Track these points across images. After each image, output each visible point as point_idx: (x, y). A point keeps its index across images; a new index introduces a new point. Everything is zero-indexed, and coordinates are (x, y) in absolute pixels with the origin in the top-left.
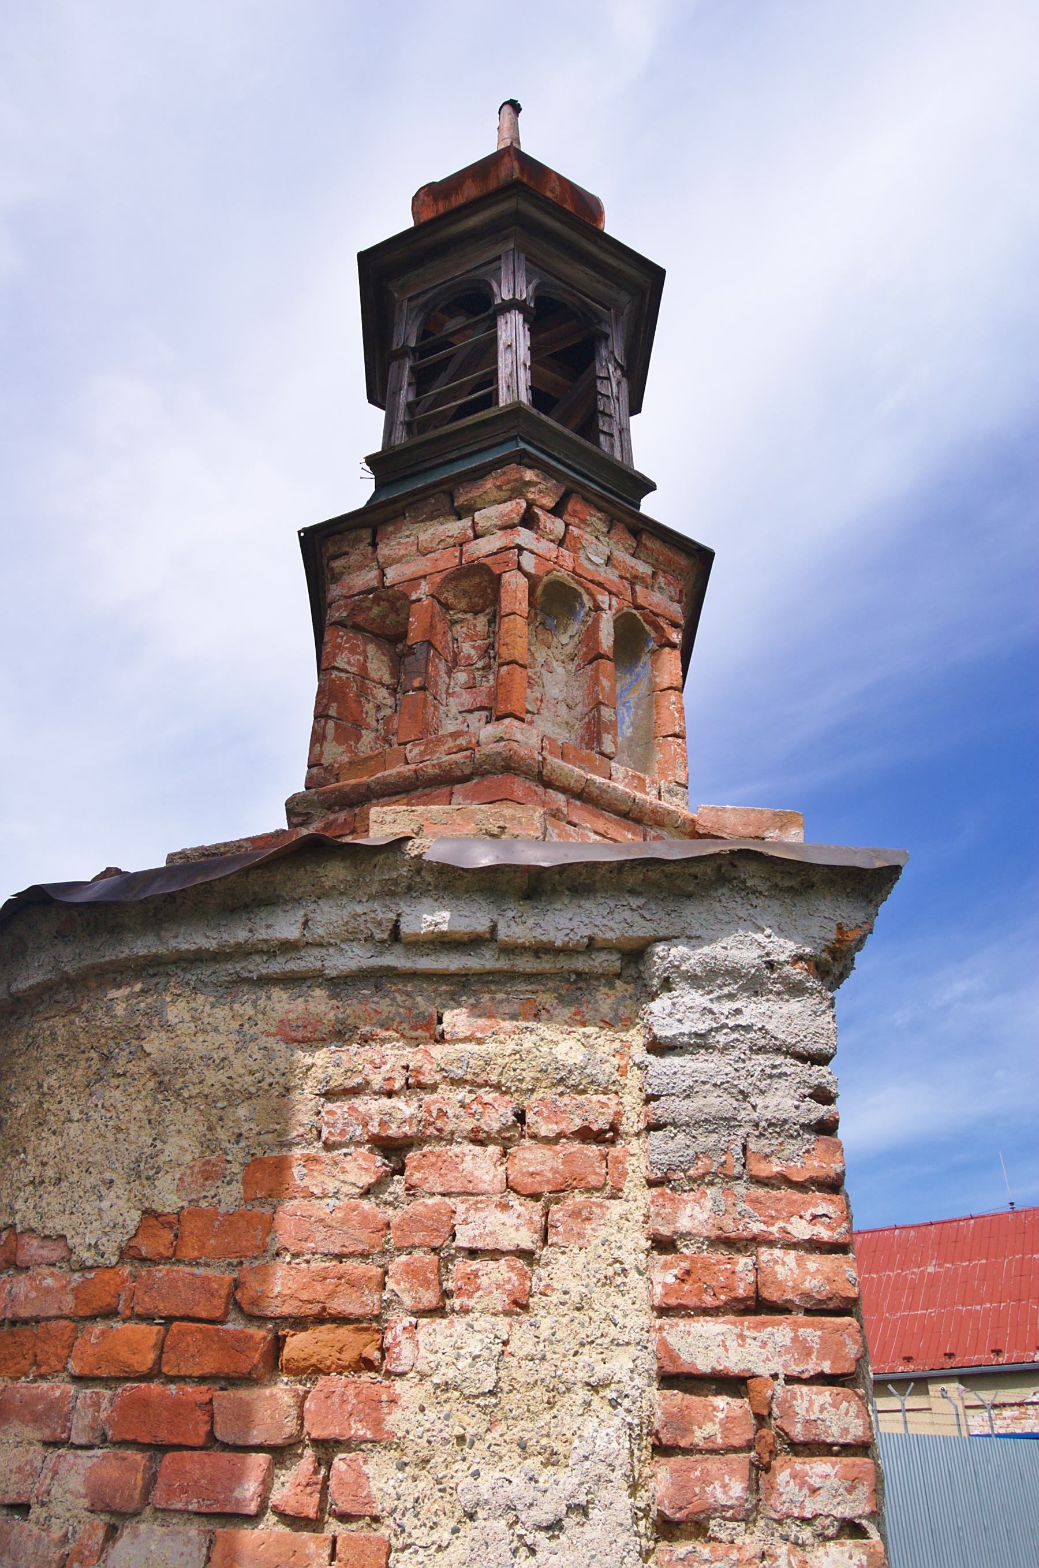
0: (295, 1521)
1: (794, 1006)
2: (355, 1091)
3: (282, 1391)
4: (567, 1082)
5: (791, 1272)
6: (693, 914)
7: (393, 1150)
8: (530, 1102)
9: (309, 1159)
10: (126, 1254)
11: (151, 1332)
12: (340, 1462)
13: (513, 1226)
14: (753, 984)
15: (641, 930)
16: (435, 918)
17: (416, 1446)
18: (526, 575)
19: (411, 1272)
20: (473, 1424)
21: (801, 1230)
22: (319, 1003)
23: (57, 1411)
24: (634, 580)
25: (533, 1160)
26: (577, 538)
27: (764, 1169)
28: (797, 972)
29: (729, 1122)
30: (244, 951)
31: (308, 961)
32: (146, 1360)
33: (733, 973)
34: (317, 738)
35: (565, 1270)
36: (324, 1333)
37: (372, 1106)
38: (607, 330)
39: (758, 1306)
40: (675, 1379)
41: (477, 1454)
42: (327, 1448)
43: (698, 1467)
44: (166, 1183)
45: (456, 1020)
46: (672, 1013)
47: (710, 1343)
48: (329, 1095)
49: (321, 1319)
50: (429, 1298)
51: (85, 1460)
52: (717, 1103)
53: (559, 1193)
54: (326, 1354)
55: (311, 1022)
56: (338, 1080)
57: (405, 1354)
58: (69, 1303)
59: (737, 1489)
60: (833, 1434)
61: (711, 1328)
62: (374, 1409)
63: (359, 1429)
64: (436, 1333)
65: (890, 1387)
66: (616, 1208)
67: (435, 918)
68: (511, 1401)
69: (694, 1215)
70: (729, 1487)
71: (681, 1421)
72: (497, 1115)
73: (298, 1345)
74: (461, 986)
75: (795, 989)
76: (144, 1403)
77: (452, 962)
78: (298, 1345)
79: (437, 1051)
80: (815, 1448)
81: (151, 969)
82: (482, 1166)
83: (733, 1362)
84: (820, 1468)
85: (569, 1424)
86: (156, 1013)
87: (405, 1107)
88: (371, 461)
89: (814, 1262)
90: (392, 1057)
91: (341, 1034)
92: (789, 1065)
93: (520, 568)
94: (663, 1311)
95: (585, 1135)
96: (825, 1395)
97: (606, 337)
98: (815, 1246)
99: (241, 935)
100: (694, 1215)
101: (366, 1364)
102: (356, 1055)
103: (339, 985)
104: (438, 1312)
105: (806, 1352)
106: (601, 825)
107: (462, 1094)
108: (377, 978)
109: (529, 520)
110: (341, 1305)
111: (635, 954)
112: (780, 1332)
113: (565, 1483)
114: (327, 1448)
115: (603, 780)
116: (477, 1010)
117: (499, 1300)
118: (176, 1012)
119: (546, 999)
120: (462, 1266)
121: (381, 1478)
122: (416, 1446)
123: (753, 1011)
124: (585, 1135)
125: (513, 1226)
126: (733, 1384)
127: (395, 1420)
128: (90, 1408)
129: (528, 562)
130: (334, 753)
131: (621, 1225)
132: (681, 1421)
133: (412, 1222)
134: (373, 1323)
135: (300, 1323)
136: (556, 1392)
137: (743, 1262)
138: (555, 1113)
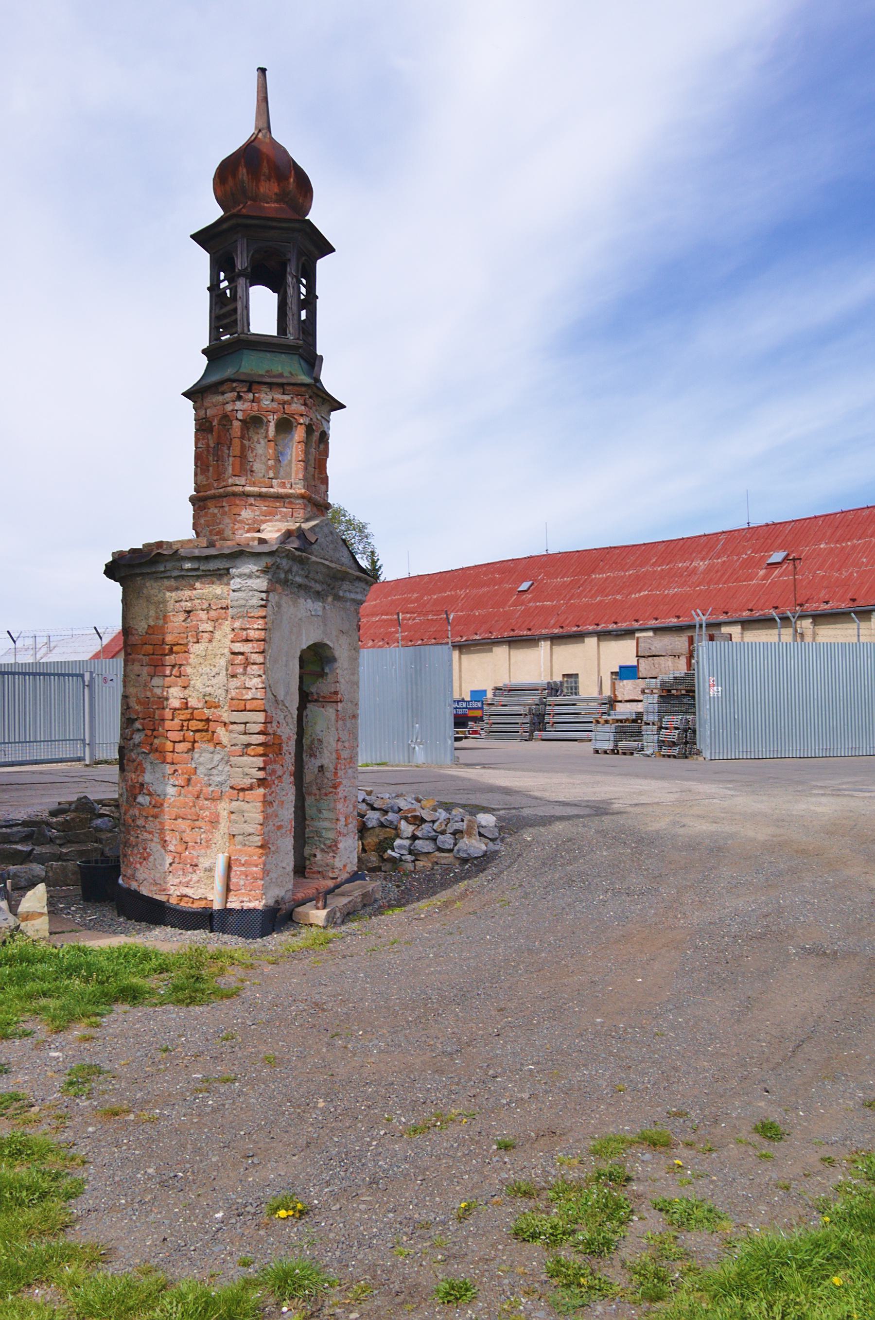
0: (176, 676)
1: (258, 580)
2: (181, 601)
3: (172, 657)
4: (218, 598)
5: (252, 634)
6: (238, 562)
7: (189, 612)
8: (212, 602)
9: (174, 615)
10: (147, 633)
11: (151, 647)
12: (182, 668)
13: (208, 627)
14: (250, 576)
15: (227, 566)
16: (188, 565)
17: (193, 665)
18: (240, 420)
19: (192, 636)
20: (202, 661)
21: (256, 626)
22: (173, 583)
23: (140, 661)
24: (284, 403)
25: (213, 614)
26: (258, 398)
27: (250, 615)
28: (258, 574)
29: (244, 606)
30: (154, 573)
31: (168, 574)
32: (151, 652)
33: (245, 575)
34: (196, 475)
35: (218, 635)
36: (179, 647)
37: (183, 604)
38: (288, 256)
39: (247, 640)
40: (233, 653)
41: (203, 666)
42: (181, 665)
43: (235, 667)
44: (150, 620)
45: (198, 585)
46: (235, 583)
47: (238, 647)
48: (176, 602)
49: (178, 644)
50: (195, 640)
51: (146, 668)
52: (242, 602)
53: (217, 620)
54: (179, 650)
55: (171, 586)
56: (177, 599)
57: (191, 650)
58: (140, 642)
59: (241, 670)
60: (258, 661)
61: (238, 644)
62: (187, 659)
63: (185, 662)
64: (197, 646)
65: (853, 614)
66: (227, 622)
67: (188, 565)
68: (208, 657)
69: (237, 624)
70: (240, 670)
71: (233, 660)
72: (205, 606)
73: (175, 648)
74: (198, 577)
75: (258, 577)
76: (152, 659)
77: (195, 573)
78: (175, 648)
79: (194, 592)
80: (254, 664)
81: (142, 574)
82: (203, 615)
83: (242, 651)
84: (255, 667)
85: (217, 660)
86: (144, 584)
87: (189, 604)
88: (204, 352)
89: (257, 632)
90: (187, 593)
91: (177, 589)
92: (256, 593)
93: (237, 419)
94: (232, 642)
95: (222, 608)
96: (257, 655)
97: (289, 260)
98: (258, 629)
99: (154, 570)
100: (237, 624)
101: (185, 652)
102: (180, 593)
103: (176, 578)
104: (198, 642)
105: (254, 648)
106: (267, 504)
107: (199, 601)
108: (183, 577)
109: (239, 398)
110: (180, 642)
111: (228, 570)
112: (250, 645)
113: (215, 670)
114: (181, 665)
115: (267, 489)
116: (202, 583)
117: (207, 640)
118: (148, 584)
119: (215, 579)
120: (201, 634)
121: (189, 670)
122: (193, 665)
123: (250, 582)
124: (222, 608)
125: (208, 627)
126: (242, 654)
127: (191, 661)
128: (146, 659)
129: (240, 415)
130: (200, 477)
131: (226, 626)
132: (233, 660)
133: (191, 627)
134: (186, 645)
135: (174, 645)
136: (215, 655)
137: (245, 632)
138: (216, 604)
